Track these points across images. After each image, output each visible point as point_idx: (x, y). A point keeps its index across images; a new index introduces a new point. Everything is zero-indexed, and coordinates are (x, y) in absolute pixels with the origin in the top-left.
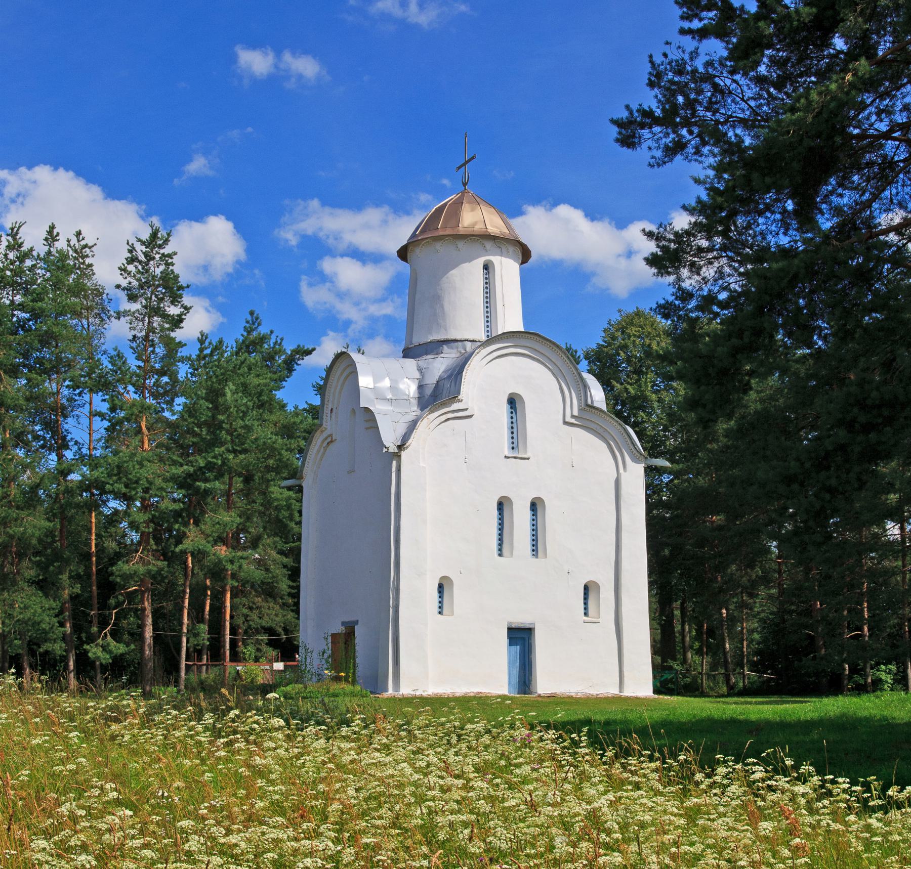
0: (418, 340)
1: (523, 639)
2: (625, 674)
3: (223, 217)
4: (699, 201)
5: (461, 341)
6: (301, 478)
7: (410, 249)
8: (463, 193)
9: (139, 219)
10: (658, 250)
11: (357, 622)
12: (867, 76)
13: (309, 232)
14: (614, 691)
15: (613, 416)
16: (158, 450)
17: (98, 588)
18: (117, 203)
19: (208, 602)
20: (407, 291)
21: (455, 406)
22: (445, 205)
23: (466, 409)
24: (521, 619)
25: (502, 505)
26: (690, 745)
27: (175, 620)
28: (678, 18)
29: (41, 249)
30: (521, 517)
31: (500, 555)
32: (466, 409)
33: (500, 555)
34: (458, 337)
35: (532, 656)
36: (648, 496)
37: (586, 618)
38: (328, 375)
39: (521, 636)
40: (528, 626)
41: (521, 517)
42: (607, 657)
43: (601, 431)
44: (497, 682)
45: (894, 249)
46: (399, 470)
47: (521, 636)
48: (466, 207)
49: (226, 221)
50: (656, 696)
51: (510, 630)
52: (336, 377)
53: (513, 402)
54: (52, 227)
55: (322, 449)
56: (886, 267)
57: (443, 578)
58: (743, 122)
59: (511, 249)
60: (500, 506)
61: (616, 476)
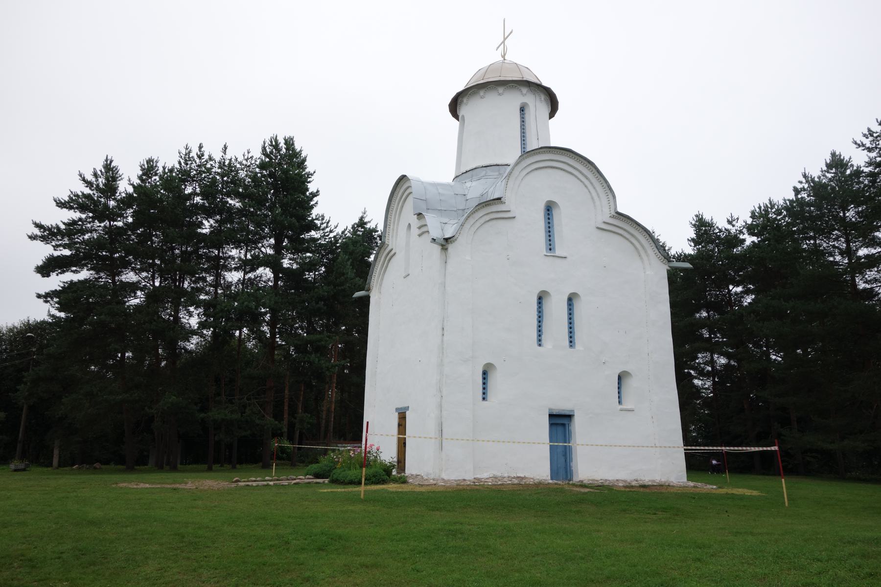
1: (564, 425)
6: (369, 290)
10: (91, 272)
11: (407, 408)
18: (780, 189)
21: (387, 251)
24: (562, 406)
27: (277, 247)
29: (217, 156)
30: (556, 309)
33: (540, 345)
35: (573, 464)
37: (621, 407)
39: (560, 422)
40: (568, 413)
41: (556, 309)
43: (596, 198)
44: (536, 466)
47: (560, 422)
50: (691, 484)
51: (551, 416)
54: (39, 296)
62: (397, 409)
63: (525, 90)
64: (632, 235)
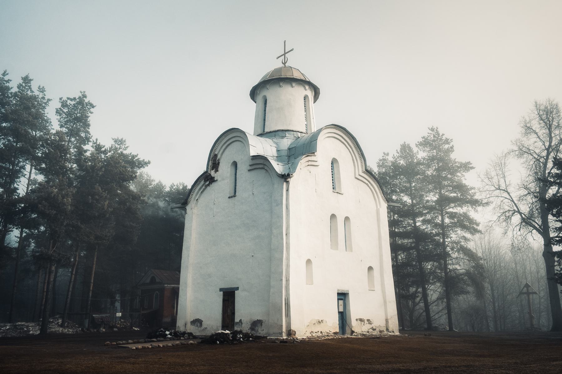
0: (267, 130)
4: (186, 186)
5: (283, 131)
9: (256, 318)
11: (237, 289)
17: (191, 344)
19: (91, 288)
24: (343, 288)
25: (333, 216)
26: (24, 162)
31: (229, 198)
34: (294, 129)
36: (392, 224)
39: (343, 296)
44: (331, 326)
45: (103, 169)
46: (287, 190)
47: (343, 296)
51: (339, 294)
52: (221, 145)
53: (309, 262)
55: (204, 187)
56: (75, 165)
62: (338, 290)
63: (307, 87)
64: (373, 187)
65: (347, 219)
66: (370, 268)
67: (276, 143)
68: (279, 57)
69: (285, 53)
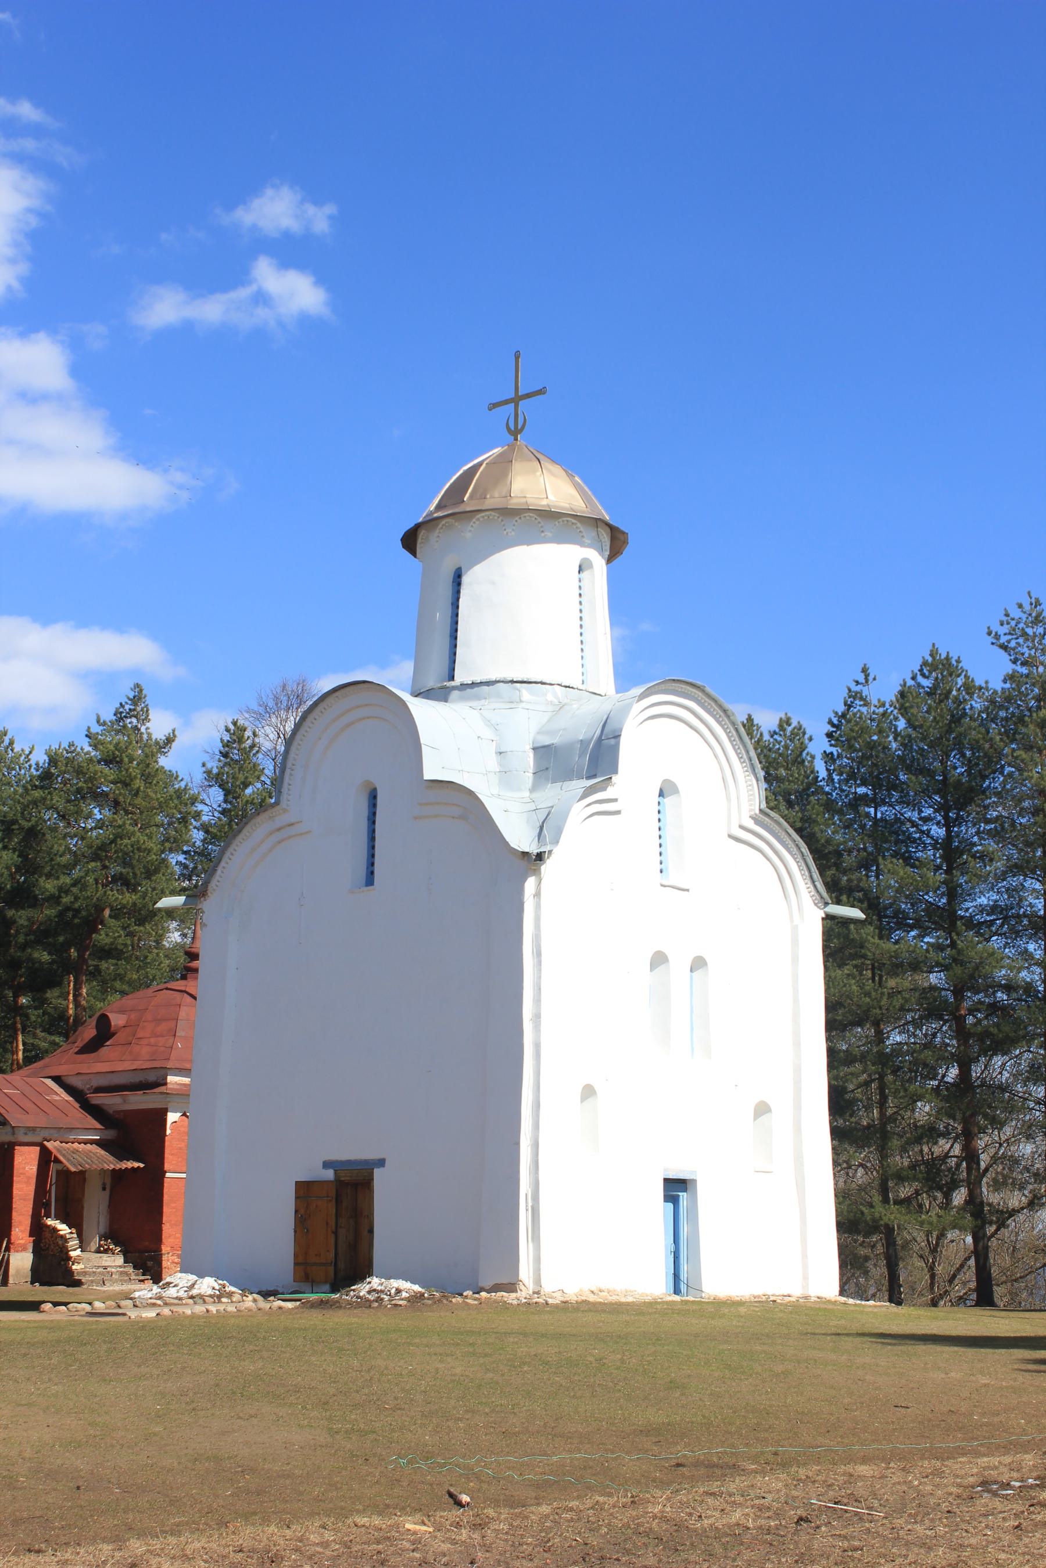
2: (947, 1349)
3: (557, 469)
7: (422, 534)
8: (512, 448)
12: (107, 947)
13: (149, 1284)
14: (649, 1282)
15: (753, 754)
16: (93, 1022)
20: (168, 1132)
22: (480, 464)
23: (616, 800)
28: (337, 1319)
32: (616, 800)
38: (289, 742)
42: (778, 1236)
48: (517, 466)
49: (58, 741)
50: (843, 1299)
53: (676, 1188)
57: (666, 781)
58: (95, 828)
59: (590, 534)
60: (370, 879)
61: (596, 817)
65: (698, 964)
66: (762, 1109)
67: (495, 727)
68: (494, 406)
69: (516, 400)
